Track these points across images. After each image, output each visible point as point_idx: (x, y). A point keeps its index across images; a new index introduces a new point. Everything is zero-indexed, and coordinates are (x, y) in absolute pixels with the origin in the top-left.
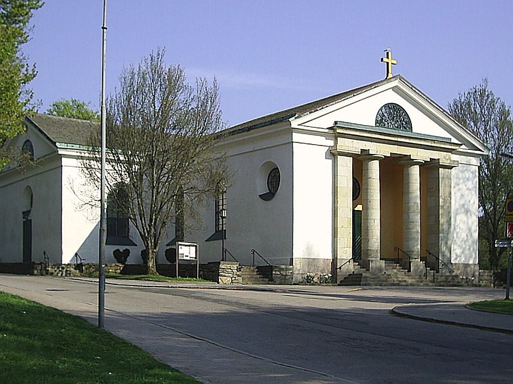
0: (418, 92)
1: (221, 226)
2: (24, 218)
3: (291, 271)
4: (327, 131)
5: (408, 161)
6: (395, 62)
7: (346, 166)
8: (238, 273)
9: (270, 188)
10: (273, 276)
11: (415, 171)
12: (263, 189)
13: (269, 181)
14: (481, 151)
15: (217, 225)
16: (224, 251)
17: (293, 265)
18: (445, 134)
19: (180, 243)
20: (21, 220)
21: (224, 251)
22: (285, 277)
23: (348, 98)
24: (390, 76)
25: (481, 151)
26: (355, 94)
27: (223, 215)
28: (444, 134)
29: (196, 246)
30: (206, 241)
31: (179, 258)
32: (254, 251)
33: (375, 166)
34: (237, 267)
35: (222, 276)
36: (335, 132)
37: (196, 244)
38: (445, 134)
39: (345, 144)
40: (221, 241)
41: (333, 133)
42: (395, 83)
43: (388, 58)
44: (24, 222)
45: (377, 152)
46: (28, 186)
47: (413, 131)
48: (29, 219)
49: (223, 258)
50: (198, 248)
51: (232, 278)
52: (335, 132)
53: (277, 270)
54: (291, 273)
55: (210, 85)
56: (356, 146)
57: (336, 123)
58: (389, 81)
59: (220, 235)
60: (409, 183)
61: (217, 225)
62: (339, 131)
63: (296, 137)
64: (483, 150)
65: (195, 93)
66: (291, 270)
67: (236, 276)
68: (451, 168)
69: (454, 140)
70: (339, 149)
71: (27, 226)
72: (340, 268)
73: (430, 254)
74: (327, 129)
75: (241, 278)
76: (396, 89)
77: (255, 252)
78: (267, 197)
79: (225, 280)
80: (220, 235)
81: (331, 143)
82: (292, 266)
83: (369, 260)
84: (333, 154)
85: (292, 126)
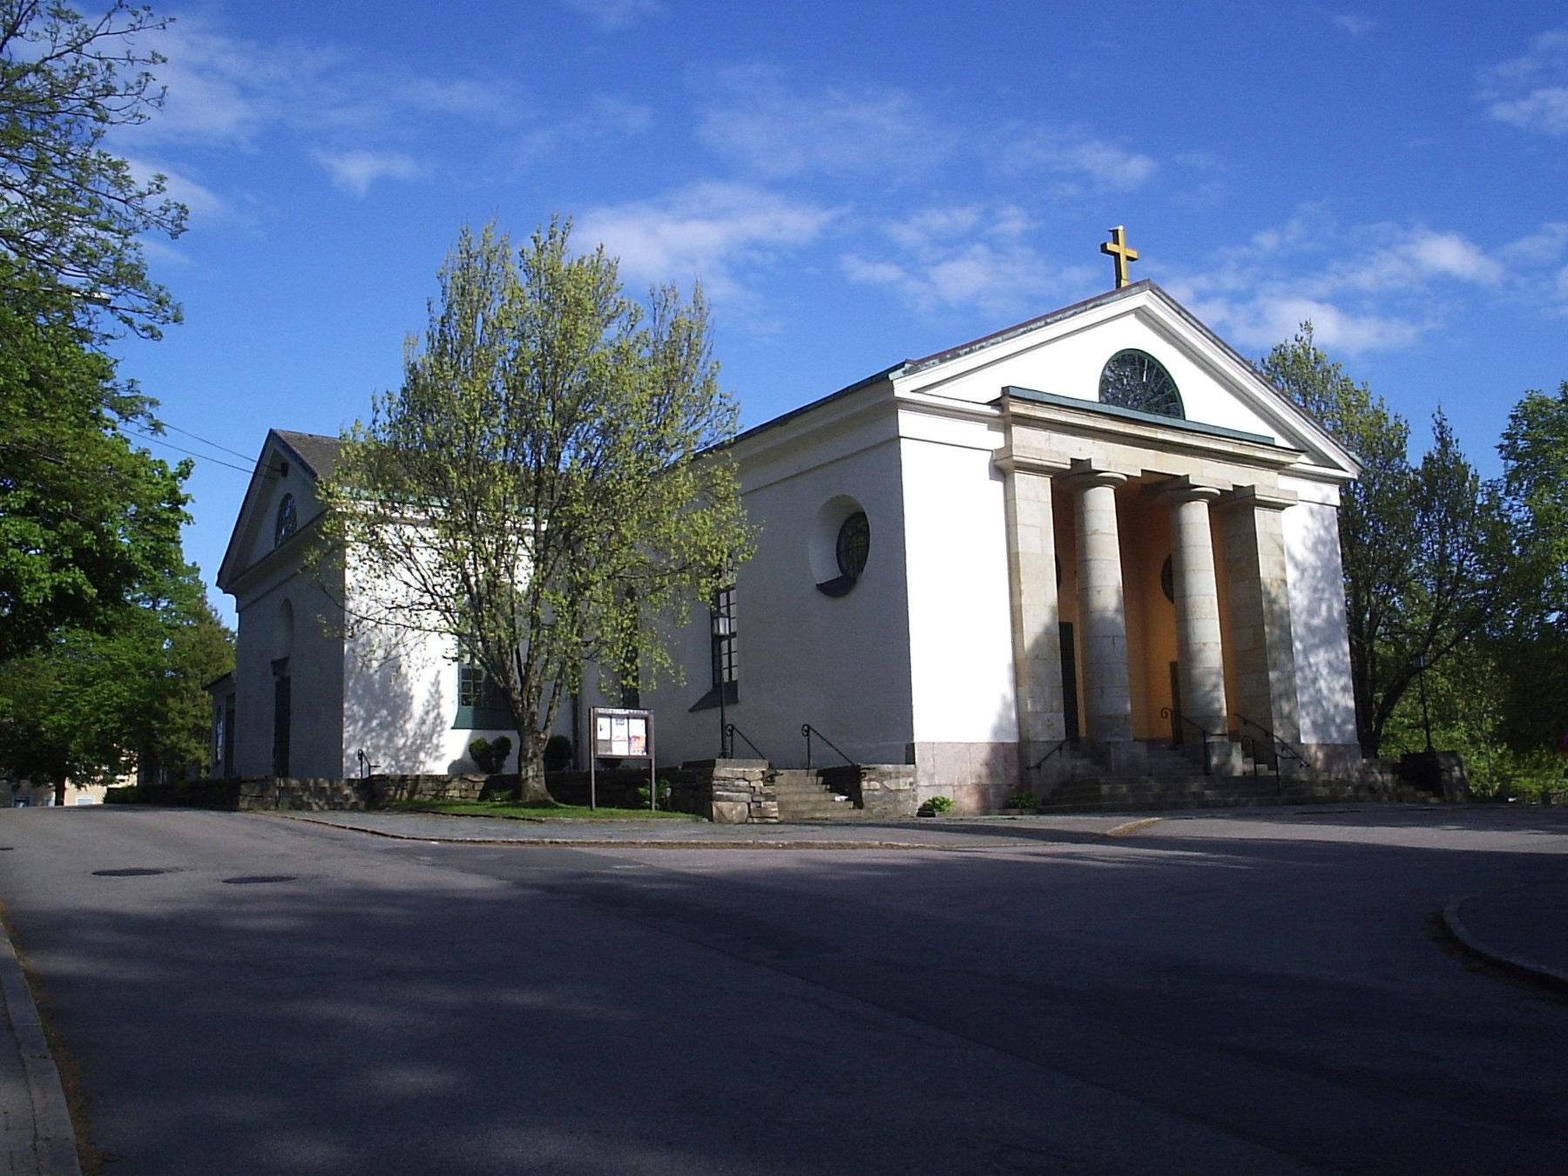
0: (1193, 322)
1: (726, 673)
2: (275, 674)
3: (911, 780)
4: (988, 409)
5: (1181, 490)
6: (1134, 254)
7: (1036, 495)
8: (767, 790)
9: (844, 565)
10: (864, 793)
11: (1197, 517)
12: (823, 567)
13: (842, 549)
14: (1344, 470)
15: (717, 670)
16: (727, 730)
17: (914, 763)
18: (1262, 429)
19: (601, 710)
20: (273, 680)
21: (727, 730)
22: (896, 796)
23: (1031, 330)
24: (1124, 284)
25: (1344, 470)
26: (1049, 321)
27: (722, 631)
28: (1256, 426)
29: (646, 719)
30: (691, 711)
31: (599, 753)
32: (809, 727)
33: (1102, 507)
34: (763, 772)
35: (721, 798)
36: (1005, 413)
37: (646, 713)
38: (1262, 429)
39: (1033, 444)
40: (719, 709)
41: (998, 417)
42: (1143, 299)
43: (1116, 242)
44: (677, 768)
45: (1110, 465)
46: (287, 600)
47: (1187, 418)
48: (287, 675)
49: (723, 747)
50: (652, 723)
51: (749, 804)
52: (1005, 413)
53: (873, 777)
54: (911, 784)
55: (686, 303)
56: (1063, 450)
57: (1005, 390)
58: (1127, 293)
59: (722, 693)
60: (1181, 547)
61: (717, 670)
62: (1017, 408)
63: (907, 422)
64: (1347, 469)
65: (645, 323)
66: (909, 776)
67: (762, 799)
68: (1280, 507)
69: (1280, 441)
70: (1019, 454)
71: (283, 690)
72: (1038, 767)
73: (1246, 722)
74: (988, 404)
75: (775, 803)
76: (1141, 313)
77: (811, 732)
78: (837, 588)
79: (731, 806)
80: (722, 693)
81: (996, 440)
82: (913, 766)
83: (1109, 743)
84: (1003, 469)
85: (897, 394)
